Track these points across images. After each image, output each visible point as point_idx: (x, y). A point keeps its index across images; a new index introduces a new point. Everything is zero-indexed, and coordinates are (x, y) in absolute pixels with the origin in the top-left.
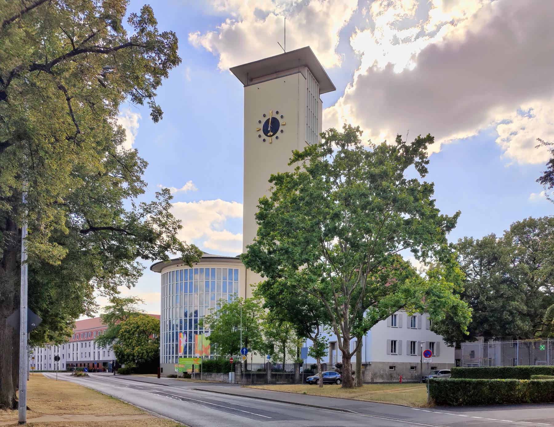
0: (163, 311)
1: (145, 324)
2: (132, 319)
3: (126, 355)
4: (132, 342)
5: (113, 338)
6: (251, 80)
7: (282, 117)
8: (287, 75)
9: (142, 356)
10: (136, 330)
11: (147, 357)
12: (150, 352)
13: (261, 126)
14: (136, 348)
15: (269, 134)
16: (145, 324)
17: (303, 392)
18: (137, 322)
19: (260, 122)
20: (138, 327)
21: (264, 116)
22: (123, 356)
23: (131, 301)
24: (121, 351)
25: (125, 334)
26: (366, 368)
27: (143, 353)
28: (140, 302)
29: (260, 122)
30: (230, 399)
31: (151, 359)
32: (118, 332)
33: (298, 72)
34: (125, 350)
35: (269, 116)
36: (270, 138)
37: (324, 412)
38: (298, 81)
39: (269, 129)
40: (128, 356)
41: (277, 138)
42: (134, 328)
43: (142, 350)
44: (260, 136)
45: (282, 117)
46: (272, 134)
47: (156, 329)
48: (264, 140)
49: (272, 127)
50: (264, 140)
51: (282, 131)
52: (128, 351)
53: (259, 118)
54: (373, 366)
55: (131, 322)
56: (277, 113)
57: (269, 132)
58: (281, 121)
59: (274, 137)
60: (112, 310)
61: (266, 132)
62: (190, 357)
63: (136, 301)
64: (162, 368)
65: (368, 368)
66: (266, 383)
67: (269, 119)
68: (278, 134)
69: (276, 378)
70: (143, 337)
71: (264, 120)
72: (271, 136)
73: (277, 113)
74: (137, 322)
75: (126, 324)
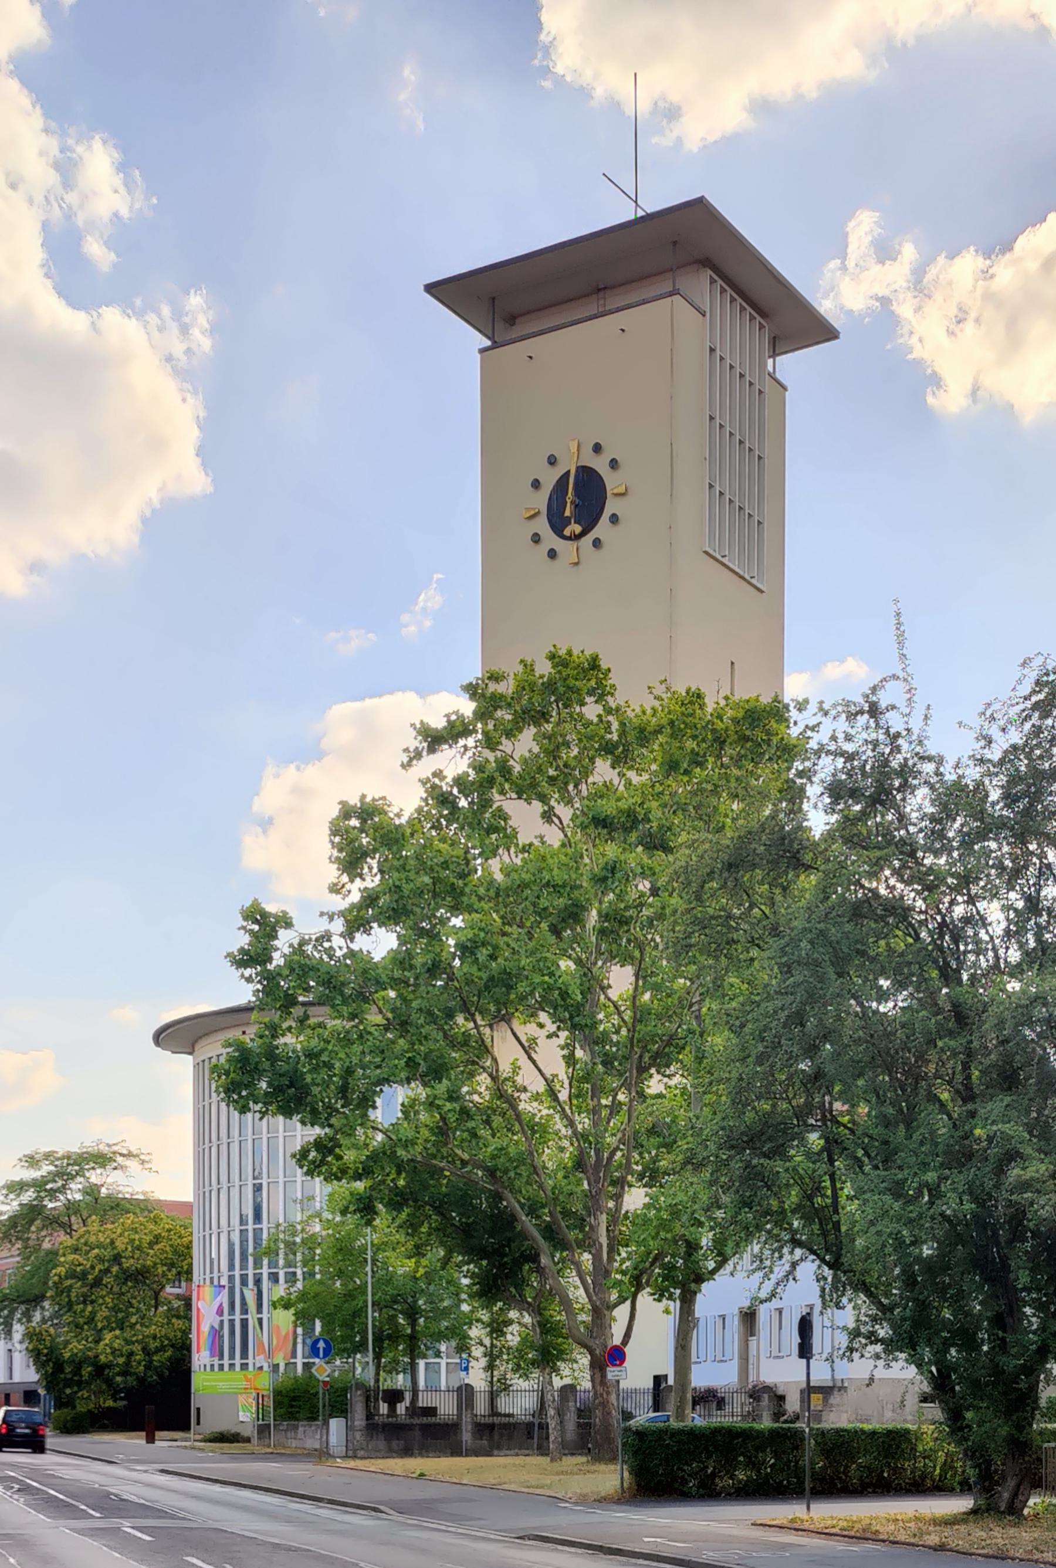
0: (196, 1195)
1: (139, 1248)
2: (97, 1231)
3: (71, 1361)
4: (93, 1313)
5: (35, 1300)
6: (512, 320)
7: (614, 464)
8: (645, 302)
9: (127, 1364)
10: (107, 1271)
11: (148, 1367)
12: (158, 1350)
13: (541, 500)
14: (108, 1337)
15: (567, 532)
16: (139, 1248)
17: (418, 1472)
18: (112, 1242)
19: (536, 484)
20: (117, 1259)
21: (552, 461)
22: (59, 1367)
23: (101, 1160)
24: (52, 1350)
25: (69, 1282)
26: (825, 1400)
27: (131, 1354)
28: (132, 1164)
29: (536, 484)
30: (196, 1497)
31: (160, 1376)
32: (47, 1277)
33: (671, 294)
34: (67, 1343)
35: (569, 464)
36: (571, 546)
37: (448, 1540)
38: (674, 329)
39: (567, 513)
40: (78, 1364)
41: (597, 543)
42: (102, 1260)
43: (128, 1342)
44: (536, 539)
45: (614, 464)
46: (578, 529)
47: (180, 1264)
48: (552, 554)
49: (580, 502)
50: (552, 554)
51: (614, 519)
52: (75, 1347)
53: (537, 472)
54: (852, 1394)
55: (93, 1239)
56: (597, 448)
57: (567, 522)
58: (612, 482)
59: (588, 540)
60: (28, 1196)
61: (558, 525)
62: (244, 1367)
63: (119, 1159)
64: (198, 1409)
65: (835, 1399)
66: (457, 1451)
67: (568, 473)
68: (602, 529)
69: (491, 1438)
70: (139, 1297)
71: (550, 479)
72: (577, 537)
73: (597, 448)
74: (112, 1242)
75: (76, 1250)
